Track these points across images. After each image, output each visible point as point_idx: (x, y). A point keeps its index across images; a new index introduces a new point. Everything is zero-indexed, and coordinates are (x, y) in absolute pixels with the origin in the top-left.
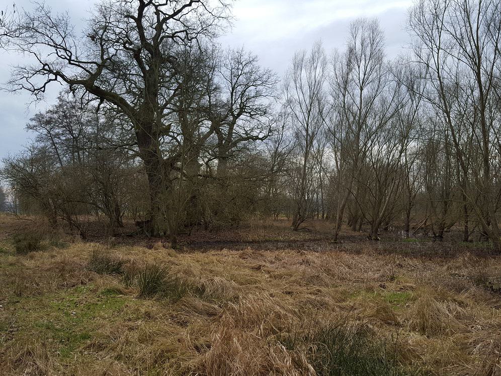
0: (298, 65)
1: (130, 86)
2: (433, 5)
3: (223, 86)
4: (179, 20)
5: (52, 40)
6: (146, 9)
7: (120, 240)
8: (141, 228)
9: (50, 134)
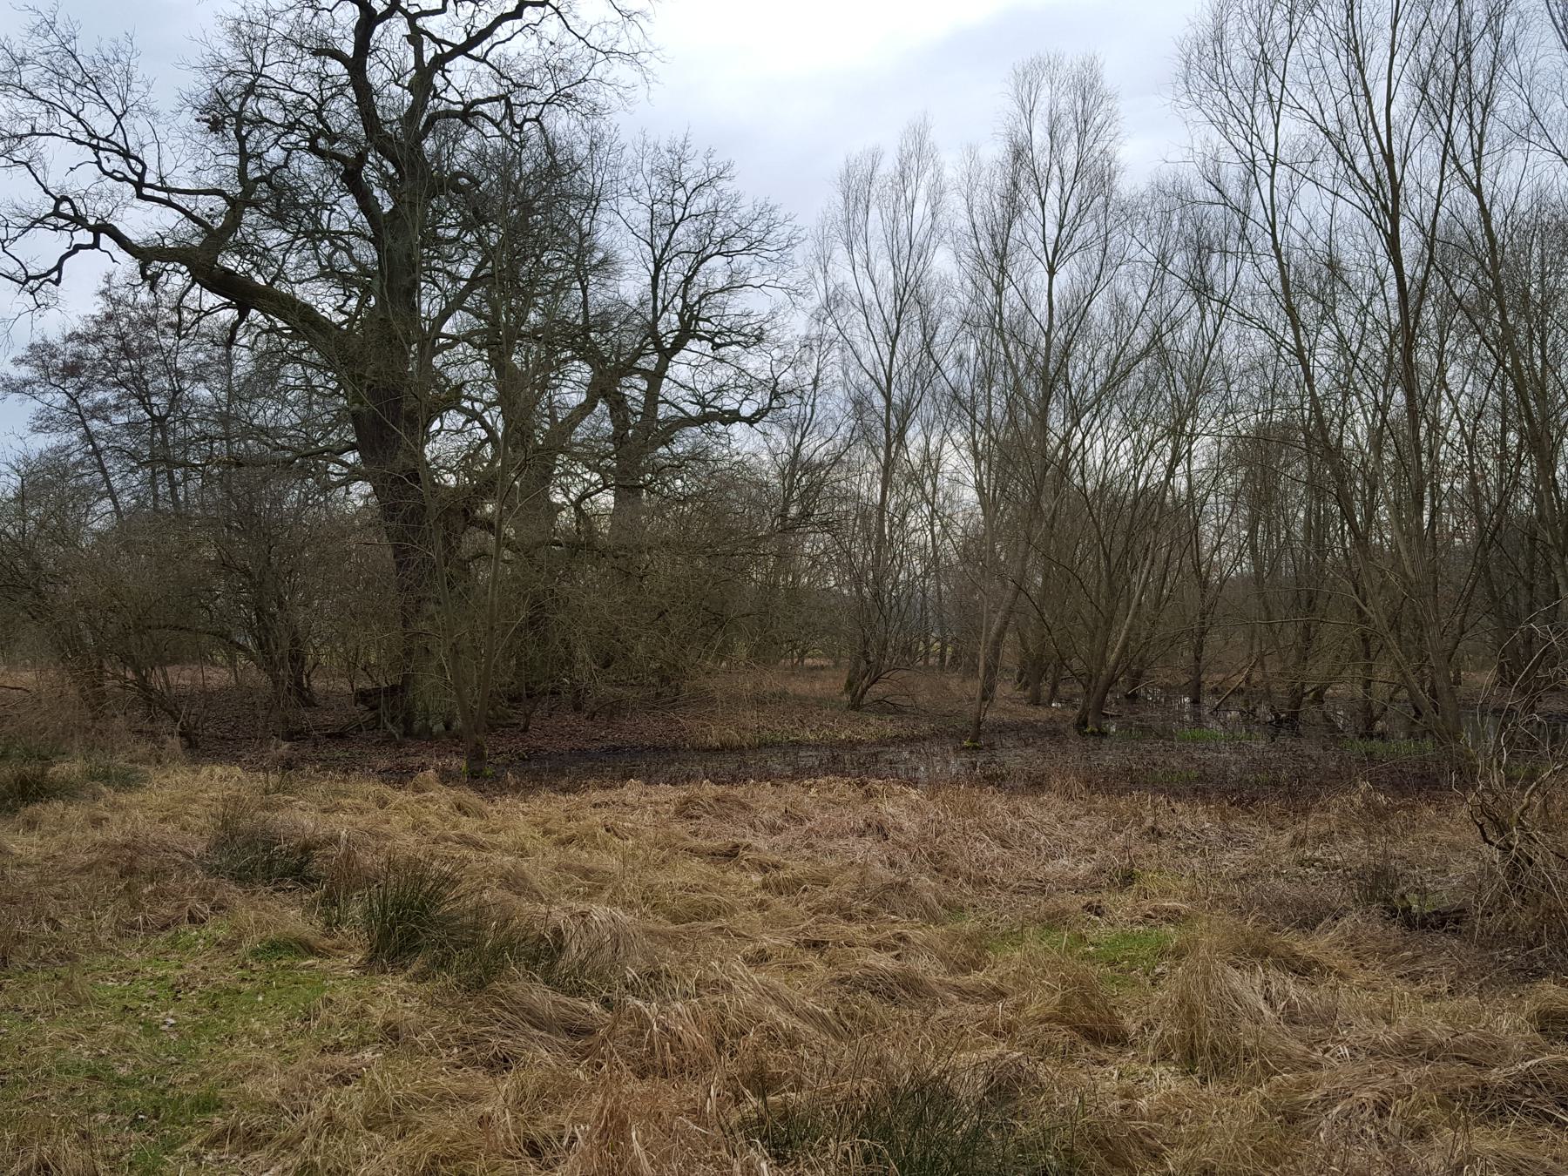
0: (856, 193)
1: (330, 257)
2: (1254, 30)
3: (626, 255)
4: (484, 60)
5: (80, 120)
6: (379, 28)
7: (308, 750)
8: (372, 709)
9: (78, 406)
